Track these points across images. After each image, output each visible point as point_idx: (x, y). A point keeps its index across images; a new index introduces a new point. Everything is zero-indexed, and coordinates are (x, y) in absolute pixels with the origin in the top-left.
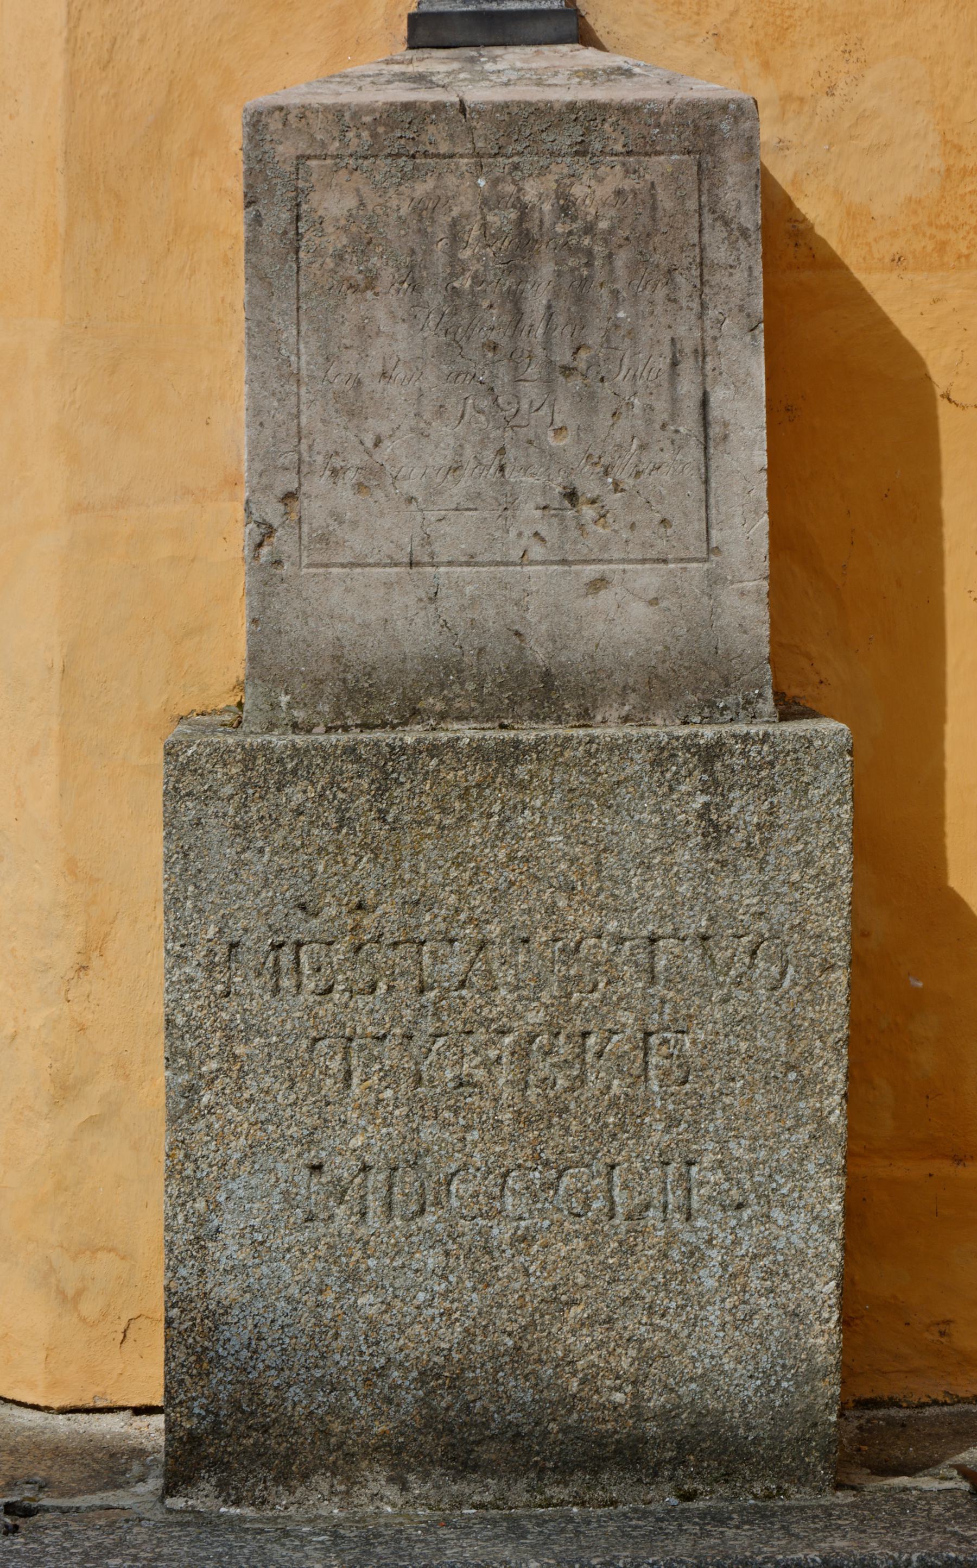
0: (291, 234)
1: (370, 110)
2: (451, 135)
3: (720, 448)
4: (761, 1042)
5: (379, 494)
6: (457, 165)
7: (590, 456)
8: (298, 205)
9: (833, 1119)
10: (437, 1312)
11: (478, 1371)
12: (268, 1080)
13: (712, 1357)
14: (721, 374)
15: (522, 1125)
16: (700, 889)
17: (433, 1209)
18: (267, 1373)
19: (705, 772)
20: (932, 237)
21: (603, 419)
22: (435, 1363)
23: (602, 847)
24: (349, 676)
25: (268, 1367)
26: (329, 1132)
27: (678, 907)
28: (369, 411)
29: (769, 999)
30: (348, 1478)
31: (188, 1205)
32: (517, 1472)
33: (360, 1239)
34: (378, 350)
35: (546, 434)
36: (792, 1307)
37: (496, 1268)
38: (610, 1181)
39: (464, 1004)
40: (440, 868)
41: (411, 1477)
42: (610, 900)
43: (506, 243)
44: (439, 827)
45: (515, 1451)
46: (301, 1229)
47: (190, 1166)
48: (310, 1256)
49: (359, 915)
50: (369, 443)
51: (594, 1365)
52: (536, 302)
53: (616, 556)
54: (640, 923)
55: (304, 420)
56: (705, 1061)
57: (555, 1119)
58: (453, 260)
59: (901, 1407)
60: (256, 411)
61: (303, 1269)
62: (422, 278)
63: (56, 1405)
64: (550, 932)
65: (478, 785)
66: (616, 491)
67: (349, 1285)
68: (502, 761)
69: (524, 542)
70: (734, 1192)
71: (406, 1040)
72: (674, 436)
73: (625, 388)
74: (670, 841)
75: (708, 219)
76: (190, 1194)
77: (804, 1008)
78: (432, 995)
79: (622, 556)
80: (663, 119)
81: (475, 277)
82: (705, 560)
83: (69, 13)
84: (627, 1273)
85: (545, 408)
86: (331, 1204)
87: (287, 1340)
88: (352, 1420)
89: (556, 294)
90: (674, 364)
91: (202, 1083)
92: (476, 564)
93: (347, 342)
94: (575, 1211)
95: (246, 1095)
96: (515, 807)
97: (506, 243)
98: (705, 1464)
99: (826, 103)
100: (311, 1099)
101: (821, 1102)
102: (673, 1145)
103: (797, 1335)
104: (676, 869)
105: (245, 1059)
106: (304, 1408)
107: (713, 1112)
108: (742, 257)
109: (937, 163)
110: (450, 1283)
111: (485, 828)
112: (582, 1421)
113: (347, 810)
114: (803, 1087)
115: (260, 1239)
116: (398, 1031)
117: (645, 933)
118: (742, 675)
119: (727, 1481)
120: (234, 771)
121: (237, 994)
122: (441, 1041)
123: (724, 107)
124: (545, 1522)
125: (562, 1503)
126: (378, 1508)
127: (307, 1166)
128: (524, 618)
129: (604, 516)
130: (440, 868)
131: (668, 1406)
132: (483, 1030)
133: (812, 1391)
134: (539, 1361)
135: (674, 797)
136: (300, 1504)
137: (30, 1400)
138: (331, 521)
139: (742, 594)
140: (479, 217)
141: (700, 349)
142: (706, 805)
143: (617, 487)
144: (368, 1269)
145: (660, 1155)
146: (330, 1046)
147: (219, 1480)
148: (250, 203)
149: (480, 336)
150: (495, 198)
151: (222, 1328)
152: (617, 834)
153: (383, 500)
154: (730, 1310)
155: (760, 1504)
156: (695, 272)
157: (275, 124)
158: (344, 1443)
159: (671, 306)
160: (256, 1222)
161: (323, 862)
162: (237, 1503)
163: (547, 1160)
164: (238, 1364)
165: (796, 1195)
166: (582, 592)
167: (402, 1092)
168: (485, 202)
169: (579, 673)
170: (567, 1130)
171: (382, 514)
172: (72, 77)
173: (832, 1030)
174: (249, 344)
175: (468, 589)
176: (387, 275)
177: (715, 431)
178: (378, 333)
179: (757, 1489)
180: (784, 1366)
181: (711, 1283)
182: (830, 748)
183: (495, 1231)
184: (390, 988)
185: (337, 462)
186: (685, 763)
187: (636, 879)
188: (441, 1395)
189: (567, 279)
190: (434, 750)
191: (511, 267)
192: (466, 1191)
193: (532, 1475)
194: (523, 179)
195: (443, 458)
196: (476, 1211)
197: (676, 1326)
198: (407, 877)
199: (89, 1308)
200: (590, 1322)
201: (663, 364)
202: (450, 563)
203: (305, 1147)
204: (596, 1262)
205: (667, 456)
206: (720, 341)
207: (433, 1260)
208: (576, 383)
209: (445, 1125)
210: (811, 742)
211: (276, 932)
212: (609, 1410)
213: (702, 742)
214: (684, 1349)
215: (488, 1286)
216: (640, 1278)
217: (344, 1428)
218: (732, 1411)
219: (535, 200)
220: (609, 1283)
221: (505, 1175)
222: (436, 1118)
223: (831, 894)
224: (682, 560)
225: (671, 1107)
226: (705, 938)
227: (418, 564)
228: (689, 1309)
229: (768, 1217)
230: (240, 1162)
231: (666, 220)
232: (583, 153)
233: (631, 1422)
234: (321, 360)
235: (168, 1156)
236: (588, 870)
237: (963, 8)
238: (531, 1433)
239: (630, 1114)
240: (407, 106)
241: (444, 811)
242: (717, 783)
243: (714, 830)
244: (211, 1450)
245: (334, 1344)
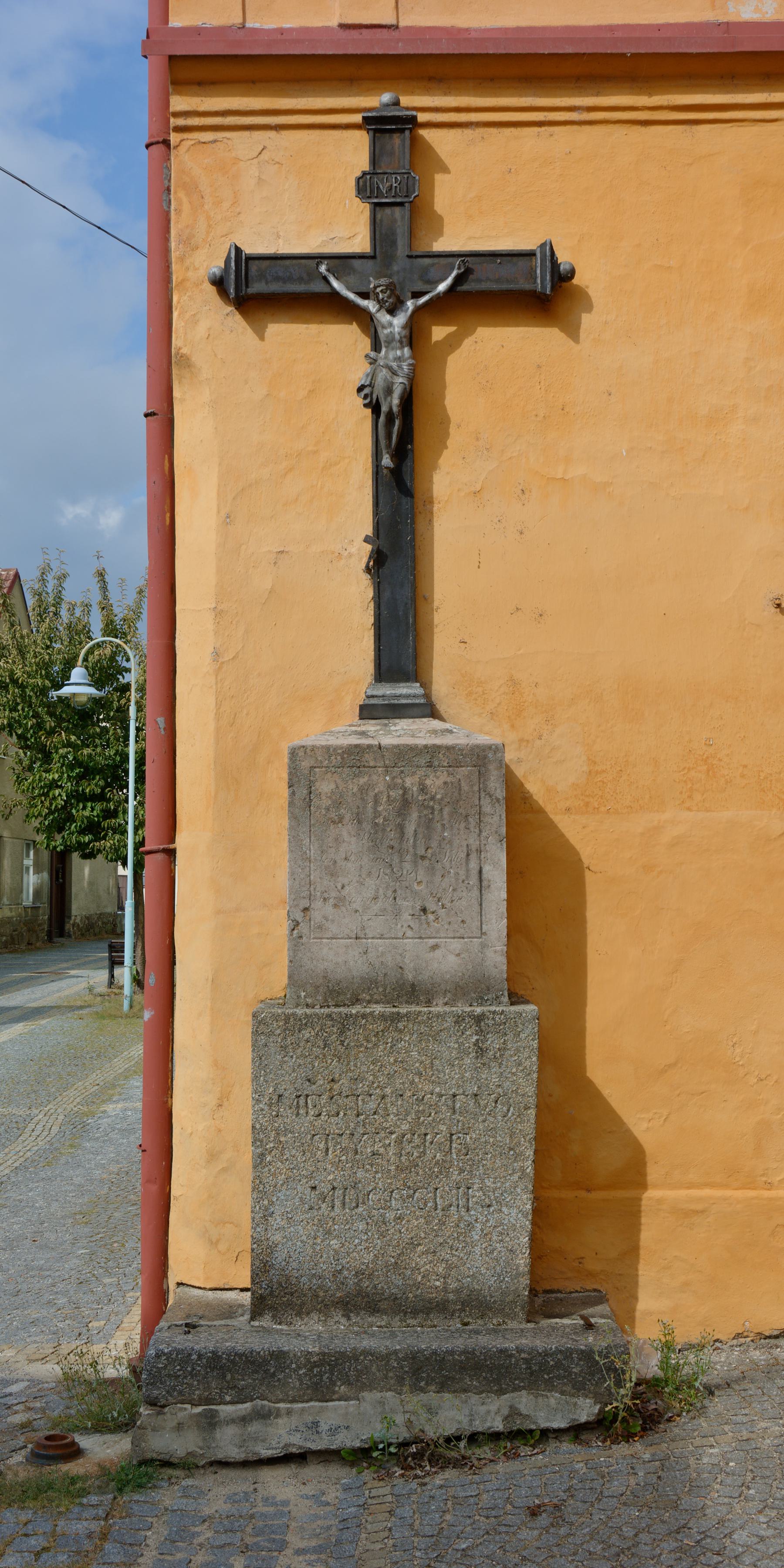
0: (308, 799)
1: (341, 747)
4: (499, 1138)
5: (343, 909)
20: (583, 800)
21: (438, 878)
32: (395, 1313)
38: (435, 1195)
41: (352, 1315)
46: (307, 1213)
47: (261, 1187)
50: (339, 887)
52: (410, 828)
55: (312, 877)
63: (208, 1287)
65: (382, 1031)
68: (392, 1021)
69: (404, 929)
73: (448, 865)
78: (362, 1117)
81: (384, 818)
82: (480, 938)
89: (418, 825)
90: (468, 855)
93: (330, 845)
99: (538, 742)
109: (585, 768)
111: (385, 1049)
122: (366, 1136)
125: (414, 1326)
142: (477, 1040)
143: (443, 907)
149: (387, 843)
160: (289, 1210)
162: (280, 1324)
168: (389, 787)
170: (418, 1173)
175: (380, 949)
176: (348, 817)
177: (485, 883)
181: (476, 1237)
184: (345, 1114)
189: (423, 819)
190: (364, 1016)
195: (370, 894)
197: (462, 1255)
199: (222, 1247)
200: (426, 1252)
201: (463, 855)
202: (373, 938)
205: (464, 894)
208: (426, 863)
209: (367, 1171)
221: (392, 1192)
226: (476, 1095)
227: (359, 938)
230: (282, 1185)
234: (319, 852)
238: (401, 1297)
239: (444, 1168)
240: (356, 746)
241: (368, 1041)
242: (482, 1031)
243: (481, 1051)
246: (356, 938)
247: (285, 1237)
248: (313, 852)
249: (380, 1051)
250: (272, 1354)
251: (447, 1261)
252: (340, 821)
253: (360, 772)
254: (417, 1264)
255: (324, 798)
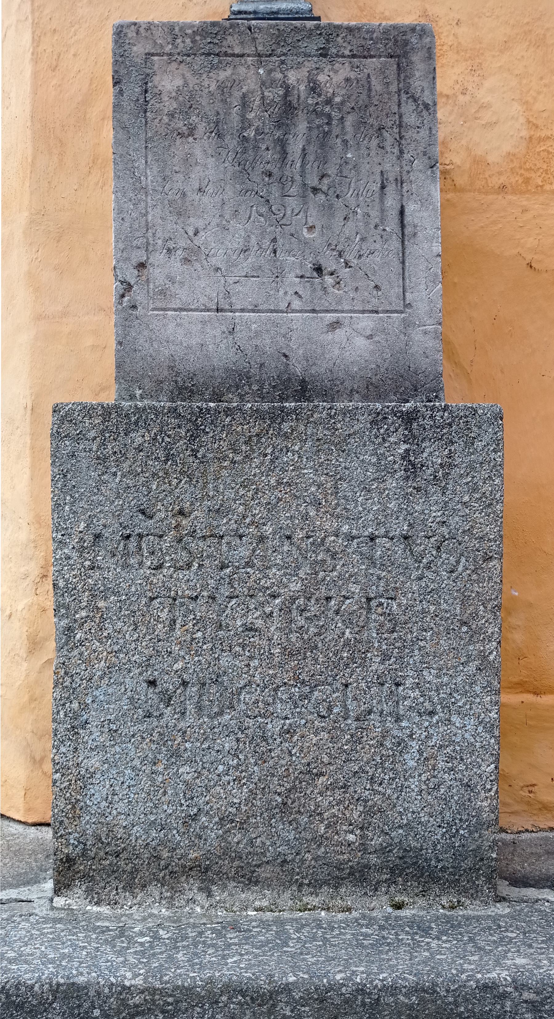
0: (141, 101)
1: (191, 26)
2: (242, 42)
3: (412, 241)
4: (444, 606)
5: (197, 265)
6: (245, 60)
7: (330, 245)
8: (146, 83)
9: (491, 657)
10: (231, 778)
11: (259, 818)
12: (120, 624)
13: (413, 812)
14: (412, 194)
15: (286, 657)
16: (403, 506)
17: (228, 711)
18: (119, 817)
19: (406, 429)
20: (522, 175)
21: (338, 221)
22: (230, 812)
23: (338, 477)
24: (179, 379)
25: (119, 813)
26: (160, 659)
27: (389, 517)
28: (190, 212)
29: (449, 578)
30: (172, 888)
31: (67, 705)
32: (286, 885)
33: (181, 729)
34: (196, 174)
35: (302, 230)
36: (466, 781)
37: (270, 751)
38: (345, 695)
39: (249, 577)
40: (232, 488)
41: (214, 888)
42: (344, 512)
43: (277, 110)
44: (231, 462)
45: (283, 871)
46: (142, 722)
47: (68, 680)
48: (148, 740)
49: (180, 518)
50: (191, 233)
51: (335, 816)
52: (295, 147)
53: (346, 308)
54: (363, 527)
55: (150, 218)
56: (407, 618)
57: (309, 654)
58: (243, 118)
59: (507, 832)
60: (120, 211)
61: (143, 749)
62: (224, 129)
63: (30, 821)
64: (304, 532)
65: (257, 435)
66: (346, 267)
67: (173, 760)
68: (273, 420)
69: (288, 298)
70: (426, 704)
71: (211, 601)
72: (383, 233)
73: (352, 203)
74: (383, 474)
75: (404, 97)
76: (68, 698)
77: (472, 584)
78: (228, 571)
79: (350, 308)
80: (375, 35)
81: (257, 130)
82: (402, 312)
83: (33, 37)
84: (357, 755)
85: (301, 213)
86: (162, 706)
87: (132, 796)
88: (175, 849)
89: (309, 142)
90: (383, 187)
91: (76, 625)
92: (259, 311)
93: (177, 168)
94: (322, 714)
95: (105, 634)
96: (282, 450)
97: (277, 110)
98: (409, 884)
99: (461, 98)
100: (148, 637)
101: (484, 647)
102: (386, 672)
103: (469, 800)
104: (387, 492)
105: (104, 610)
106: (143, 841)
107: (413, 651)
108: (425, 122)
109: (524, 133)
110: (240, 759)
111: (262, 463)
112: (327, 853)
113: (171, 449)
114: (472, 636)
115: (115, 728)
116: (205, 594)
117: (366, 533)
118: (425, 384)
119: (424, 896)
120: (97, 422)
121: (98, 567)
122: (234, 601)
123: (413, 29)
124: (303, 926)
125: (314, 908)
126: (192, 909)
127: (146, 681)
128: (288, 345)
129: (339, 283)
130: (232, 488)
131: (384, 844)
132: (261, 594)
133: (480, 837)
134: (299, 812)
135: (386, 445)
136: (140, 904)
137: (17, 817)
138: (167, 282)
139: (426, 333)
140: (260, 93)
141: (399, 178)
142: (407, 451)
143: (347, 265)
144: (186, 750)
145: (378, 679)
146: (160, 603)
147: (87, 887)
148: (116, 83)
150: (269, 81)
151: (89, 787)
152: (348, 469)
153: (200, 269)
154: (425, 782)
155: (448, 913)
156: (396, 130)
157: (131, 33)
158: (169, 864)
159: (380, 151)
160: (112, 717)
161: (156, 483)
162: (98, 904)
163: (304, 680)
164: (99, 811)
165: (468, 707)
166: (325, 330)
167: (208, 634)
168: (263, 83)
169: (323, 381)
170: (316, 660)
171: (199, 278)
172: (35, 75)
173: (491, 599)
174: (115, 168)
175: (254, 326)
176: (201, 128)
177: (408, 230)
178: (196, 163)
179: (444, 901)
180: (461, 820)
181: (412, 763)
182: (488, 415)
183: (270, 726)
184: (200, 566)
185: (171, 244)
186: (393, 423)
187: (361, 498)
188: (234, 833)
189: (315, 133)
191: (279, 124)
192: (250, 699)
193: (295, 888)
194: (287, 70)
195: (237, 243)
196: (256, 712)
197: (389, 791)
198: (211, 494)
201: (376, 187)
202: (242, 310)
203: (144, 668)
204: (336, 748)
205: (378, 246)
206: (412, 173)
207: (228, 744)
208: (321, 197)
209: (236, 656)
210: (476, 411)
211: (124, 528)
212: (345, 846)
213: (404, 409)
214: (394, 806)
215: (265, 762)
216: (365, 759)
217: (170, 854)
218: (427, 849)
219: (295, 83)
220: (344, 762)
221: (276, 690)
222: (230, 651)
223: (490, 510)
224: (387, 311)
225: (384, 647)
226: (406, 538)
227: (222, 310)
228: (397, 780)
229: (449, 721)
230: (101, 678)
231: (377, 97)
232: (324, 55)
233: (360, 854)
234: (160, 180)
235: (55, 673)
236: (329, 492)
237: (538, 46)
238: (293, 860)
239: (358, 653)
241: (235, 451)
242: (414, 437)
243: (413, 468)
244: (82, 868)
245: (163, 799)
246: (217, 310)
247: (106, 762)
248: (151, 177)
249: (253, 468)
250: (55, 990)
251: (366, 801)
252: (191, 134)
253: (220, 62)
254: (317, 806)
255: (166, 99)
